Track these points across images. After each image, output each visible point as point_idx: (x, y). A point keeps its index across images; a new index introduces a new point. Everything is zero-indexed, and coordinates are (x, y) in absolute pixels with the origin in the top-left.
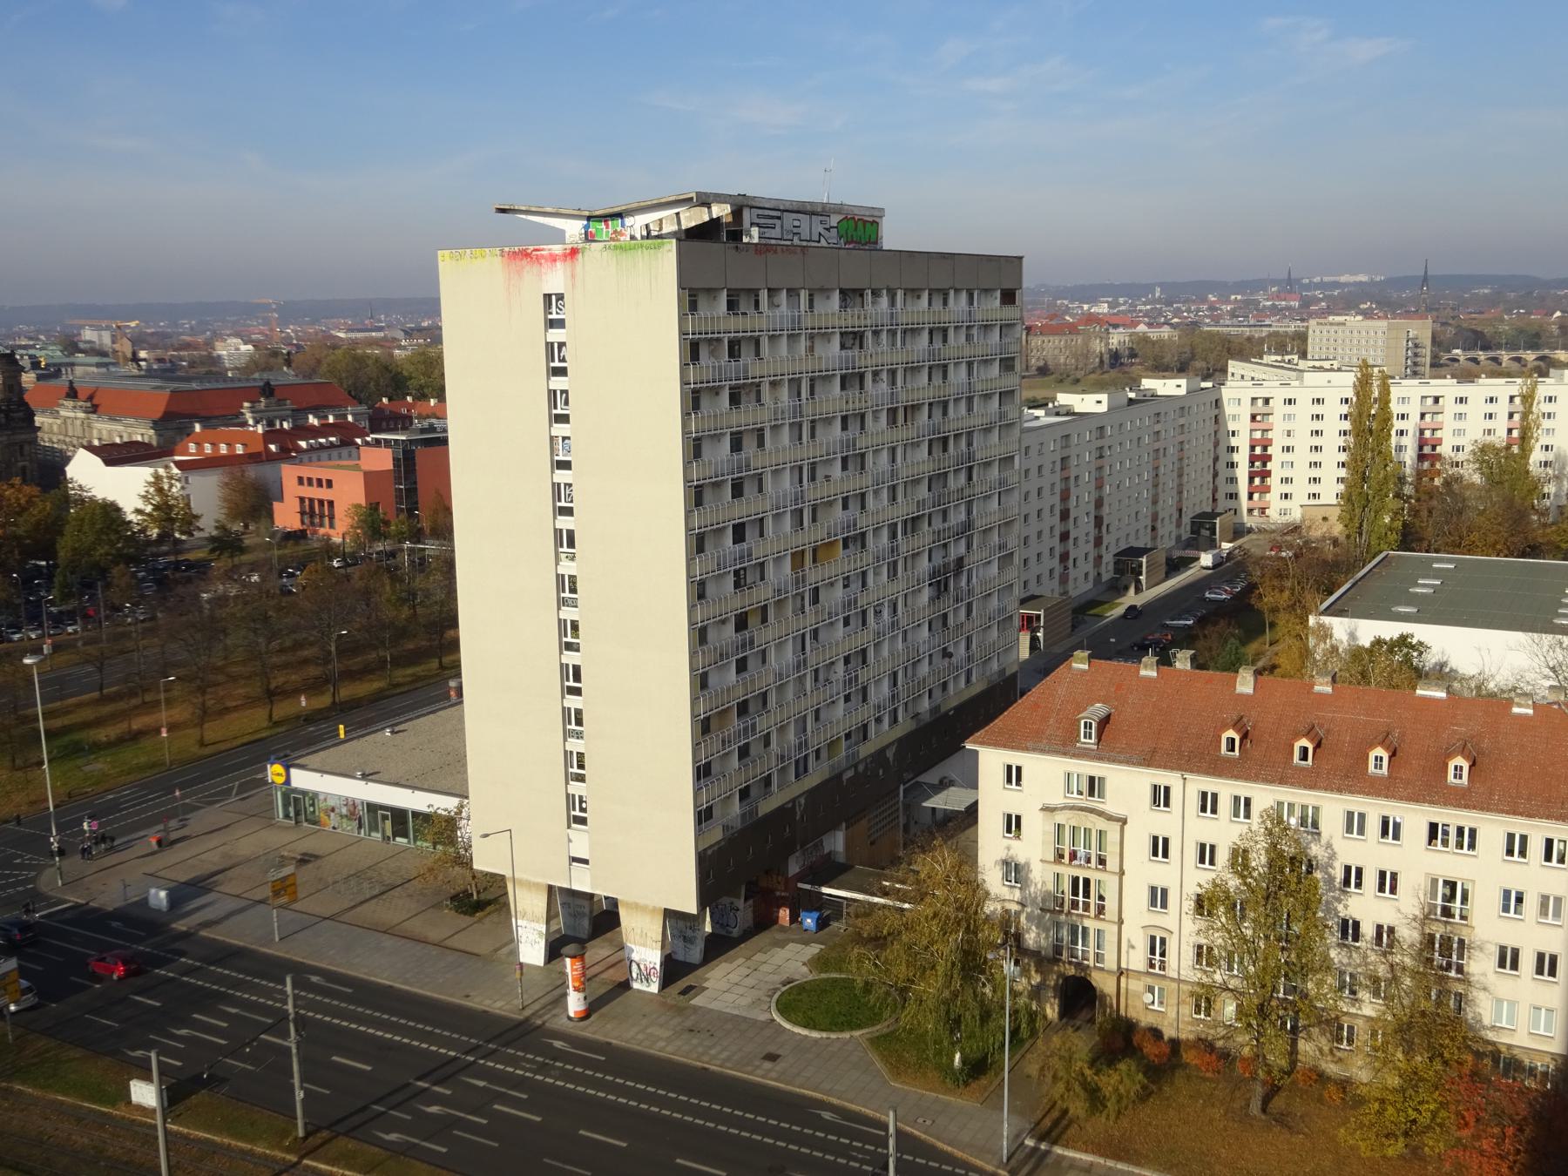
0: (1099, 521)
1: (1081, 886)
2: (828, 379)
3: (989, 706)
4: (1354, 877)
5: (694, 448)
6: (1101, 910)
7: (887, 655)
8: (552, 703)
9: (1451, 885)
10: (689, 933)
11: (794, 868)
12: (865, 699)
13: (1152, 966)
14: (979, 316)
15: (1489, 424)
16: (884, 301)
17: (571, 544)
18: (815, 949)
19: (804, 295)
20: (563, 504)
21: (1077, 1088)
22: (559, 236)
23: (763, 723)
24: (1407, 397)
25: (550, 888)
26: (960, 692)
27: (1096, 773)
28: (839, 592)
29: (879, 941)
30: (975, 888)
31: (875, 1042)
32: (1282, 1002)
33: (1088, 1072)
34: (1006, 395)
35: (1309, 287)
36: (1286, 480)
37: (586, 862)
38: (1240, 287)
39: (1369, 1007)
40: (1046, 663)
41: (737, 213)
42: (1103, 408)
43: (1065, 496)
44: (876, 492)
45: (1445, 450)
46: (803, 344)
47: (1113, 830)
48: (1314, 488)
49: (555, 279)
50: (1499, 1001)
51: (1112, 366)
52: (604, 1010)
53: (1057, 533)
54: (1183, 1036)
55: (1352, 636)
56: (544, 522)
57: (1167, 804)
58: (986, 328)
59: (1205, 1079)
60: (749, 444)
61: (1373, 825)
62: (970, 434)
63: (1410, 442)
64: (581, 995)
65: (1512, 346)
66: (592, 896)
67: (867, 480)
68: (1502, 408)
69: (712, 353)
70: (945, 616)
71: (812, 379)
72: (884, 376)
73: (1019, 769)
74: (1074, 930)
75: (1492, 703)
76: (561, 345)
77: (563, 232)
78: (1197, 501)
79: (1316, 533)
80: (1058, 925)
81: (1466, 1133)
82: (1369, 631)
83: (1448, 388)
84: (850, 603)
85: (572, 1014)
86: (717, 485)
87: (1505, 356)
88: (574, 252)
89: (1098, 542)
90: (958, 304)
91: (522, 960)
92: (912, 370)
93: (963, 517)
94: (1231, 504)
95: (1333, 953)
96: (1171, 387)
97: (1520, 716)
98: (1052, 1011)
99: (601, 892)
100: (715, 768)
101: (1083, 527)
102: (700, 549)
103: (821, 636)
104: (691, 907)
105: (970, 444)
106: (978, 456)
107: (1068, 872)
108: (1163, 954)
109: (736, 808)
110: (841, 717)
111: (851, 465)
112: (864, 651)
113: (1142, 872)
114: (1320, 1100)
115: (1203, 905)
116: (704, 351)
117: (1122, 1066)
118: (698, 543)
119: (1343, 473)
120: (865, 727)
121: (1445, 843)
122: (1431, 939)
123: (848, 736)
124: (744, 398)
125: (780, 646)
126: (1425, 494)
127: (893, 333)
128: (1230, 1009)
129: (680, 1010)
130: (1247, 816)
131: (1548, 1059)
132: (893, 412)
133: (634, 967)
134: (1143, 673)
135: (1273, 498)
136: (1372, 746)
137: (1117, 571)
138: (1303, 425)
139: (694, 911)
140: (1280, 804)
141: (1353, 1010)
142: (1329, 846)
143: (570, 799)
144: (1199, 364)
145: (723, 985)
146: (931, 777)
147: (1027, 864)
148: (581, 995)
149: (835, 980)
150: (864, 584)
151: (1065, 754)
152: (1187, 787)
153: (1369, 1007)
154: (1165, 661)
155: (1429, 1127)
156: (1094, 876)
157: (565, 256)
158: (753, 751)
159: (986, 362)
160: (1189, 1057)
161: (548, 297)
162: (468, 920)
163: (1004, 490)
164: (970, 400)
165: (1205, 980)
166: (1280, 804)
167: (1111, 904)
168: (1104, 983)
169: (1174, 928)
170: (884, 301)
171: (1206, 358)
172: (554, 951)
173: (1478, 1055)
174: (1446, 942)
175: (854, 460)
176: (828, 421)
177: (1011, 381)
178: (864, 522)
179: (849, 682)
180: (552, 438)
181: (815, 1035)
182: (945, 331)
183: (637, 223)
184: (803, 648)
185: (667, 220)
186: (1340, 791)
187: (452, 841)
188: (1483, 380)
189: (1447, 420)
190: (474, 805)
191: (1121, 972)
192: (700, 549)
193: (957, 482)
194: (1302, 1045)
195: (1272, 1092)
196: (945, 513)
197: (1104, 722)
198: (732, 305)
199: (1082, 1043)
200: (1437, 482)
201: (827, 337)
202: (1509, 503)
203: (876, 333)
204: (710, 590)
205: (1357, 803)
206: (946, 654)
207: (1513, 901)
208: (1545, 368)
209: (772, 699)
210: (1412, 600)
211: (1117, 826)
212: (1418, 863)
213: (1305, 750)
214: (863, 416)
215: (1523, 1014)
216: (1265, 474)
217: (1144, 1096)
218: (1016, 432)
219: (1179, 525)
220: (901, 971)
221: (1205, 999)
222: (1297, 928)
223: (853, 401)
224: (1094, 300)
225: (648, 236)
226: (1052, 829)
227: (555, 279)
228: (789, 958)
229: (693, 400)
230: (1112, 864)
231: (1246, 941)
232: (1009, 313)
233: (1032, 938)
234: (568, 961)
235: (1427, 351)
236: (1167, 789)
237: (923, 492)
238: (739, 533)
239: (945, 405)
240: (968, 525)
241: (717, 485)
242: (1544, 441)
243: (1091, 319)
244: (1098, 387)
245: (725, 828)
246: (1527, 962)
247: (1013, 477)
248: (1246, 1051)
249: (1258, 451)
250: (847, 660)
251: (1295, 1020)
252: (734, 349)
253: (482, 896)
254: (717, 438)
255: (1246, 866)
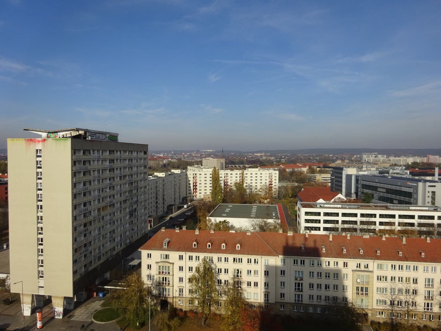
0: (164, 199)
1: (165, 279)
2: (106, 170)
3: (143, 241)
4: (220, 271)
5: (74, 185)
6: (169, 284)
7: (119, 231)
8: (35, 247)
9: (238, 270)
10: (70, 302)
11: (97, 282)
12: (114, 241)
13: (180, 295)
14: (139, 157)
15: (236, 179)
16: (119, 153)
17: (41, 208)
18: (102, 302)
19: (101, 151)
20: (39, 199)
21: (165, 326)
22: (40, 136)
23: (90, 249)
24: (222, 173)
25: (33, 295)
26: (136, 238)
27: (167, 254)
28: (108, 217)
29: (119, 298)
30: (142, 283)
31: (118, 322)
32: (207, 300)
33: (168, 322)
34: (145, 173)
35: (201, 152)
36: (200, 190)
37: (43, 287)
38: (188, 152)
39: (224, 298)
40: (155, 231)
41: (85, 133)
42: (164, 176)
43: (157, 194)
44: (117, 194)
45: (229, 183)
46: (100, 162)
47: (171, 266)
48: (205, 191)
49: (39, 146)
50: (248, 293)
51: (164, 167)
52: (47, 325)
53: (155, 202)
54: (187, 310)
55: (215, 221)
56: (34, 203)
57: (182, 259)
58: (141, 159)
59: (192, 319)
60: (88, 184)
61: (223, 259)
62: (137, 181)
63: (222, 182)
64: (41, 322)
65: (238, 164)
66: (44, 296)
67: (115, 192)
68: (238, 176)
69: (79, 164)
70: (132, 221)
71: (102, 170)
72: (119, 169)
73: (150, 254)
74: (163, 289)
75: (242, 233)
76: (40, 161)
77: (41, 135)
78: (183, 195)
79: (207, 200)
80: (160, 288)
81: (244, 322)
82: (219, 219)
83: (229, 172)
84: (111, 219)
85: (38, 327)
86: (80, 194)
87: (237, 166)
88: (44, 140)
89: (164, 204)
90: (135, 154)
91: (24, 315)
92: (125, 168)
93: (136, 199)
94: (190, 195)
95: (217, 287)
96: (177, 171)
97: (248, 235)
98: (159, 309)
99: (47, 294)
100: (78, 260)
101: (160, 200)
102: (75, 208)
103: (104, 227)
104: (71, 295)
105: (137, 184)
106: (139, 186)
107: (161, 276)
108: (182, 292)
109: (83, 269)
110: (109, 245)
111: (111, 189)
112: (114, 230)
113: (177, 274)
114: (216, 320)
115: (190, 280)
116: (77, 164)
117: (175, 319)
118: (75, 207)
119: (211, 188)
120: (114, 247)
121: (237, 262)
122: (235, 282)
123: (110, 250)
124: (86, 174)
125: (94, 230)
126: (226, 193)
127: (121, 160)
128: (197, 302)
129: (68, 322)
130: (199, 260)
131: (258, 304)
132: (121, 177)
133: (56, 313)
134: (176, 231)
135: (198, 193)
136: (222, 243)
137: (167, 209)
138: (203, 179)
139: (72, 296)
140: (205, 257)
141: (221, 299)
142: (215, 265)
143: (39, 272)
144: (182, 167)
145: (79, 314)
146: (129, 258)
147: (346, 286)
148: (41, 322)
149: (107, 309)
150: (114, 215)
151: (160, 250)
152: (186, 255)
153: (224, 298)
154: (181, 228)
155: (237, 322)
156: (167, 276)
157: (42, 141)
158: (87, 255)
159: (141, 166)
160: (189, 314)
161: (37, 150)
162: (8, 306)
163: (145, 193)
164: (137, 174)
165: (192, 297)
166: (205, 257)
167: (171, 283)
168: (170, 300)
169: (185, 286)
170: (119, 153)
171: (183, 165)
172: (33, 311)
173: (245, 305)
174: (238, 282)
175: (112, 187)
176: (106, 179)
177: (146, 170)
178: (114, 201)
179: (111, 237)
180: (37, 183)
181: (103, 323)
182: (132, 160)
183: (61, 134)
184: (100, 230)
185: (68, 134)
186: (216, 253)
187: (4, 285)
188: (235, 170)
189: (229, 178)
190: (11, 276)
191: (173, 297)
192: (75, 208)
193: (134, 192)
194: (212, 308)
195: (206, 319)
196: (132, 198)
197: (169, 242)
198: (84, 153)
199: (166, 315)
200: (228, 190)
201: (106, 161)
202: (241, 194)
203: (117, 160)
204: (78, 218)
205: (220, 255)
206: (133, 229)
207: (249, 272)
208: (245, 168)
209: (92, 243)
210: (226, 213)
211: (172, 265)
212: (232, 266)
213: (209, 245)
214: (114, 178)
215: (252, 294)
216: (196, 189)
217: (180, 325)
218: (147, 181)
219: (180, 199)
220: (124, 304)
221: (191, 301)
222: (210, 283)
223: (112, 174)
224: (160, 154)
225: (63, 137)
226: (158, 267)
227: (39, 146)
228: (96, 305)
229: (74, 174)
230: (171, 273)
231: (200, 287)
232: (145, 156)
233: (155, 292)
234: (38, 313)
235: (224, 165)
236: (182, 256)
237: (127, 194)
238: (85, 204)
239: (132, 175)
240: (137, 201)
241: (80, 194)
242: (246, 182)
243: (160, 157)
244: (162, 172)
245: (80, 275)
246: (252, 284)
247: (146, 190)
248: (201, 311)
249: (195, 184)
250: (110, 232)
251: (210, 303)
252: (84, 163)
253: (13, 299)
254: (80, 183)
255: (199, 271)
